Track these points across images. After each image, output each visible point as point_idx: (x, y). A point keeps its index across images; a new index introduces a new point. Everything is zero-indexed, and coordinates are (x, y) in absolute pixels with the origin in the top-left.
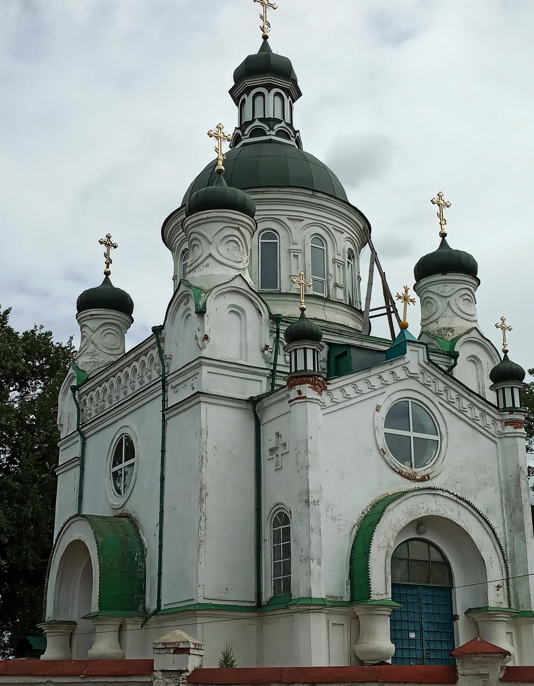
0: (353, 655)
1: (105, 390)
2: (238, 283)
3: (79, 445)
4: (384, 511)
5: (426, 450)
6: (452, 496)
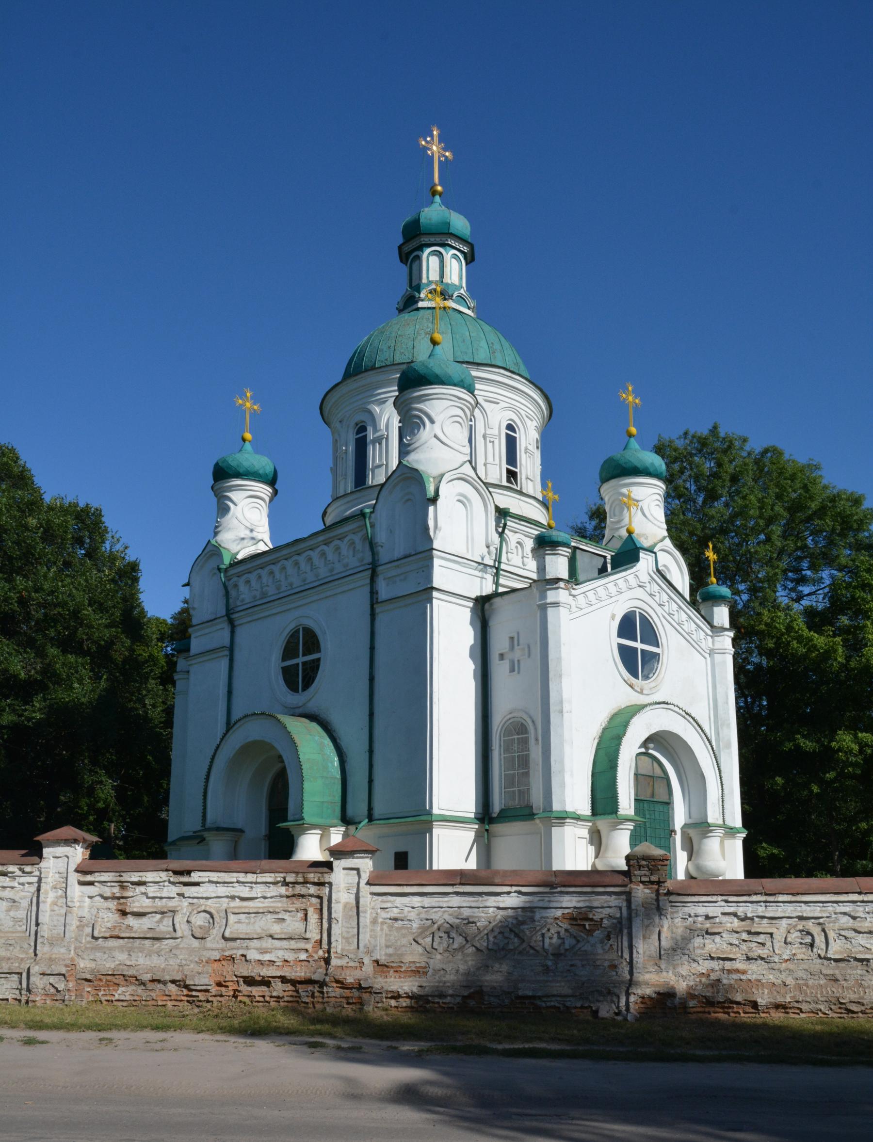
3: (227, 633)
6: (681, 711)
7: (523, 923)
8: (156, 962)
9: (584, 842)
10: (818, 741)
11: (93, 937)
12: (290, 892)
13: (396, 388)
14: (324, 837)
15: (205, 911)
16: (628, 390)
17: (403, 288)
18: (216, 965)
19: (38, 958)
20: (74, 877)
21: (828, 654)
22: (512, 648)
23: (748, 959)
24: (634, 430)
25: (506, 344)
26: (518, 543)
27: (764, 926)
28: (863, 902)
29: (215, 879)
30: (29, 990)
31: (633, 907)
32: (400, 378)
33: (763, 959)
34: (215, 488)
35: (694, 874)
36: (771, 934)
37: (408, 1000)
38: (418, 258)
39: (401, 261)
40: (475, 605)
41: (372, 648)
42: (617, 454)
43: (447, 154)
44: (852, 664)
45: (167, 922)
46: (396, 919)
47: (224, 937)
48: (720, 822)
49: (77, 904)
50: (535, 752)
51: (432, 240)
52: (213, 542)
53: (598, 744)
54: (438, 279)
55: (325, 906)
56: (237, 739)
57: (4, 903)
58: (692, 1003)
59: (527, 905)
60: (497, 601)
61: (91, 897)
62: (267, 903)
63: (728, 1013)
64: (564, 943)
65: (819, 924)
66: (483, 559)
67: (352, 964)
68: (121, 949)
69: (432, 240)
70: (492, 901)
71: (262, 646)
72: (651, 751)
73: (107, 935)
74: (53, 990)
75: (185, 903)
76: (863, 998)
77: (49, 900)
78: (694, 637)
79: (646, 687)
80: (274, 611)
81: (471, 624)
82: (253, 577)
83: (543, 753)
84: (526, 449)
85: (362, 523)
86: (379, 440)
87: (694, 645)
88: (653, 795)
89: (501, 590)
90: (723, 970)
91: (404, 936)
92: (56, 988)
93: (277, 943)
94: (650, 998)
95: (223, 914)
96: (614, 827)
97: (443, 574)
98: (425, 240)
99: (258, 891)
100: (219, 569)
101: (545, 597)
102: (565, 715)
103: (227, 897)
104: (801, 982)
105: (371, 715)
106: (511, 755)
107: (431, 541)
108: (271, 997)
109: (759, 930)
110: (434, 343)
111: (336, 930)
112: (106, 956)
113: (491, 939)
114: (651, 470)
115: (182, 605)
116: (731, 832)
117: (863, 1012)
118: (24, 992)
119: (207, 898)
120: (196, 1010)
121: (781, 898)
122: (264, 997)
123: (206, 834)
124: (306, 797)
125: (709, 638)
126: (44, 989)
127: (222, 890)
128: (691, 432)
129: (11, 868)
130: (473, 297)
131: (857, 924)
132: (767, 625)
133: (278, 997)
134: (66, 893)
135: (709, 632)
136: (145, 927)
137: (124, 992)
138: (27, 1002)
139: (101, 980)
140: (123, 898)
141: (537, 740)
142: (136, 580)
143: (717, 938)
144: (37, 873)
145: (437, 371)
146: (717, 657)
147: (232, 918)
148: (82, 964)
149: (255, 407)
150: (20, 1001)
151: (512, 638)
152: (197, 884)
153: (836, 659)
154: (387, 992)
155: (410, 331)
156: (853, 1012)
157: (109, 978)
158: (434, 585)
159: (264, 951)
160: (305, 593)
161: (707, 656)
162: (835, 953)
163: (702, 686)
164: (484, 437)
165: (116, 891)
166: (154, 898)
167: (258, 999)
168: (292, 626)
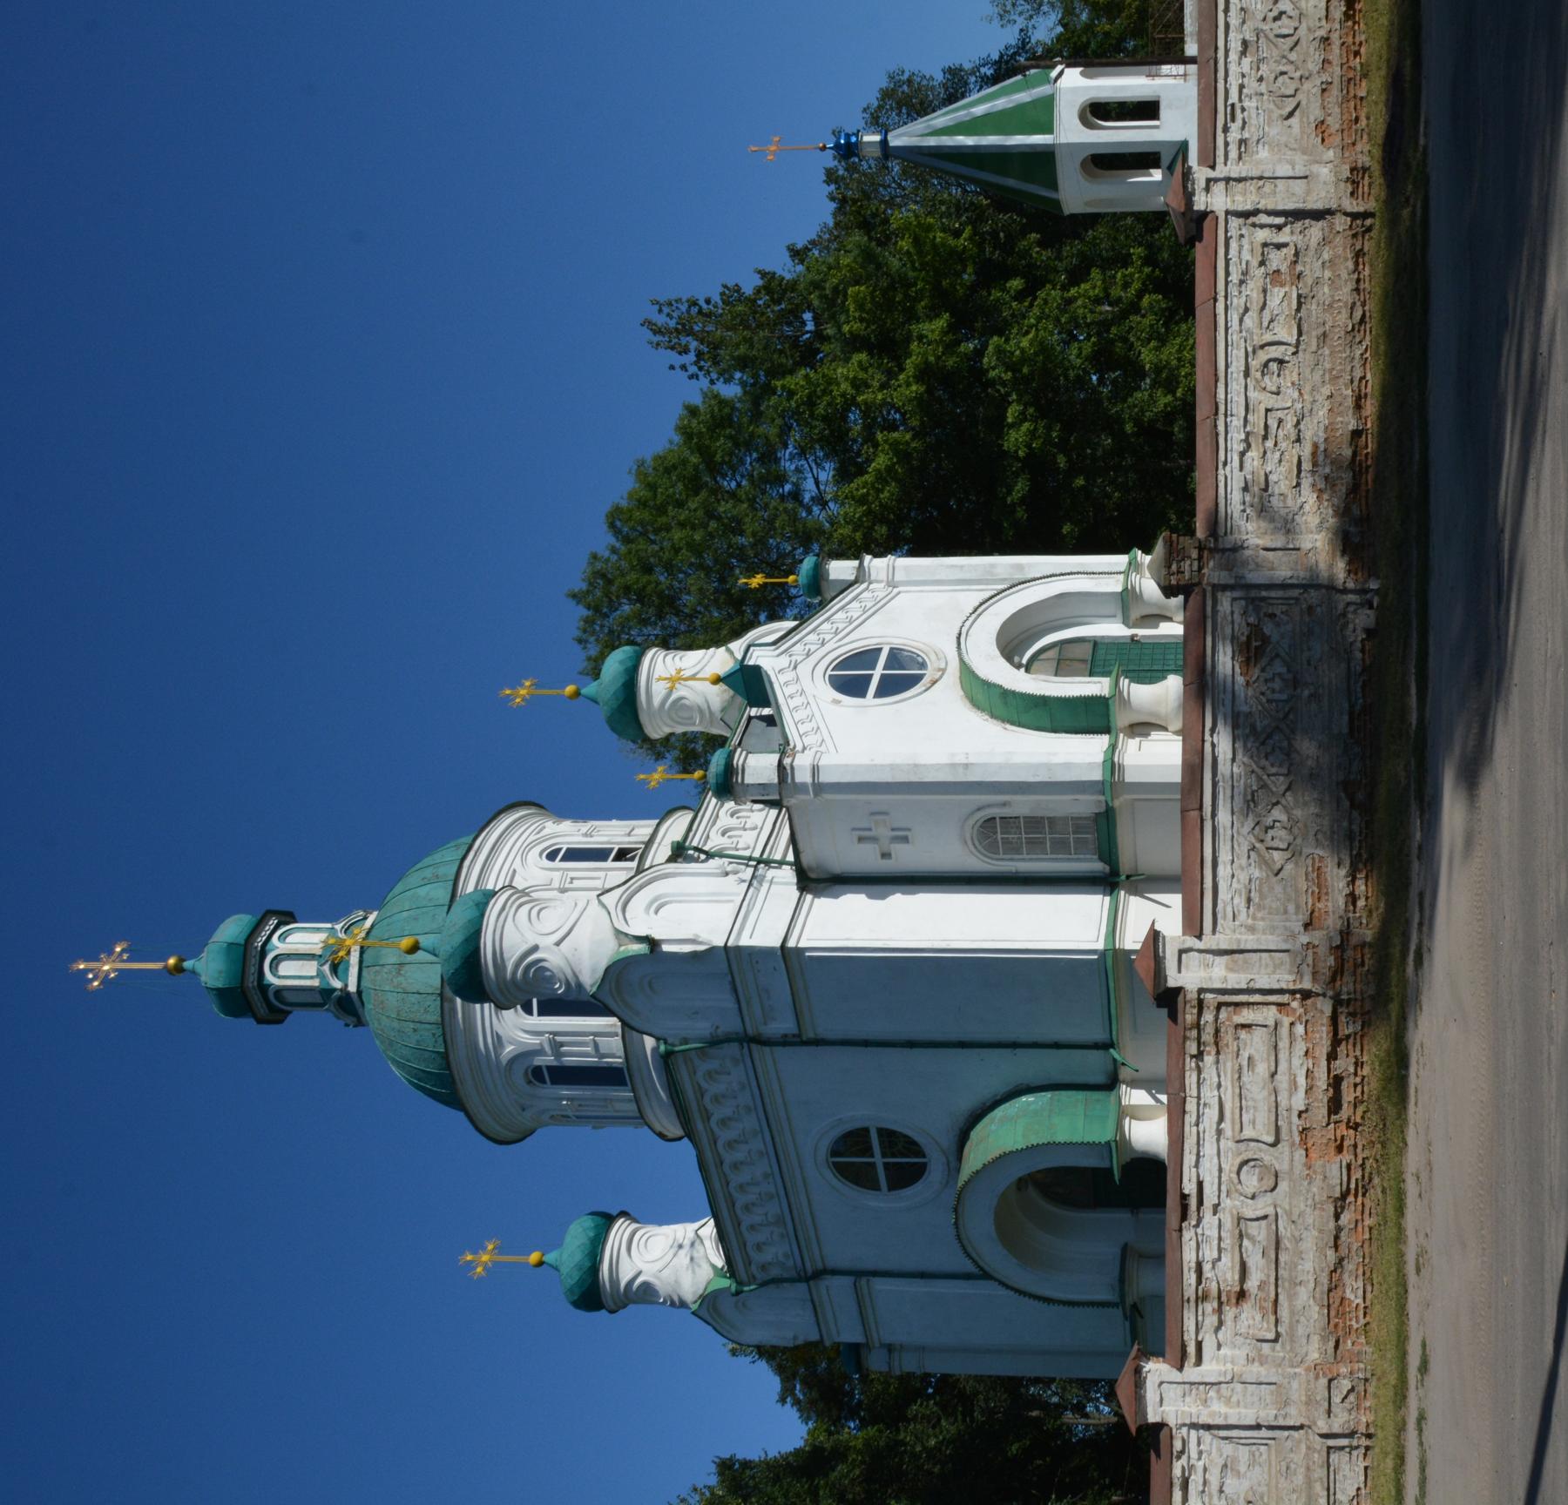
7: (1253, 727)
8: (1309, 1243)
9: (1146, 744)
10: (1016, 475)
11: (1275, 1340)
12: (1211, 1049)
13: (478, 1006)
14: (1137, 1113)
15: (1238, 1173)
17: (325, 1019)
18: (1313, 1155)
19: (1306, 1423)
20: (1191, 1373)
21: (902, 454)
22: (874, 839)
23: (1298, 440)
24: (570, 689)
25: (427, 861)
26: (723, 834)
27: (1257, 419)
28: (1226, 297)
29: (1194, 1158)
30: (1351, 1435)
31: (1232, 581)
32: (464, 998)
33: (1298, 423)
34: (613, 1307)
36: (1267, 410)
37: (1358, 883)
38: (279, 991)
39: (280, 1022)
40: (809, 891)
41: (866, 1043)
42: (603, 712)
44: (915, 423)
45: (1253, 1228)
46: (1249, 900)
47: (1274, 1145)
48: (1121, 577)
49: (1229, 1366)
50: (1022, 806)
51: (253, 970)
52: (694, 1307)
53: (1012, 723)
54: (315, 963)
55: (1231, 999)
56: (994, 1256)
57: (1228, 1481)
58: (1356, 511)
59: (1229, 721)
60: (806, 860)
61: (1219, 1346)
62: (1227, 1083)
63: (1368, 467)
64: (1280, 674)
65: (1254, 352)
67: (1310, 960)
68: (1292, 1297)
69: (253, 970)
70: (1224, 768)
71: (855, 1224)
72: (1024, 661)
73: (1272, 1318)
74: (1352, 1398)
75: (1227, 1203)
77: (1224, 1409)
79: (936, 665)
80: (805, 1204)
81: (836, 897)
82: (752, 1239)
83: (1023, 793)
84: (586, 835)
85: (680, 1059)
86: (556, 1046)
87: (879, 606)
88: (1084, 661)
89: (790, 857)
90: (1313, 472)
91: (1271, 889)
92: (1349, 1392)
93: (1283, 1067)
94: (1349, 563)
95: (1242, 1146)
96: (1126, 703)
97: (764, 933)
98: (251, 980)
99: (1209, 1095)
100: (738, 1293)
101: (804, 785)
102: (972, 760)
103: (1218, 1140)
105: (962, 1045)
106: (1025, 841)
107: (713, 949)
108: (1356, 1074)
110: (415, 948)
111: (1263, 982)
112: (1302, 1319)
113: (1274, 770)
114: (630, 664)
115: (788, 1405)
117: (1363, 305)
118: (1355, 1443)
119: (1220, 1170)
120: (1376, 1180)
122: (1356, 1085)
123: (1129, 1301)
124: (1077, 1139)
126: (1350, 1411)
127: (1209, 1149)
128: (578, 633)
129: (1177, 1472)
130: (348, 913)
131: (1255, 307)
132: (855, 530)
133: (1356, 1064)
134: (1213, 1384)
135: (864, 586)
136: (1262, 1262)
137: (1353, 1291)
138: (1369, 1436)
139: (1336, 1326)
140: (1219, 1297)
141: (1004, 804)
142: (746, 1464)
143: (1273, 478)
144: (1185, 1430)
145: (458, 939)
147: (1248, 1133)
148: (1314, 1356)
149: (490, 1247)
150: (1367, 1448)
152: (1200, 1184)
153: (907, 443)
154: (1346, 911)
155: (392, 1000)
156: (1364, 316)
157: (1333, 1313)
158: (778, 944)
159: (1294, 1084)
160: (780, 1153)
163: (937, 598)
165: (1210, 1307)
166: (1220, 1250)
167: (1358, 1093)
168: (830, 1175)
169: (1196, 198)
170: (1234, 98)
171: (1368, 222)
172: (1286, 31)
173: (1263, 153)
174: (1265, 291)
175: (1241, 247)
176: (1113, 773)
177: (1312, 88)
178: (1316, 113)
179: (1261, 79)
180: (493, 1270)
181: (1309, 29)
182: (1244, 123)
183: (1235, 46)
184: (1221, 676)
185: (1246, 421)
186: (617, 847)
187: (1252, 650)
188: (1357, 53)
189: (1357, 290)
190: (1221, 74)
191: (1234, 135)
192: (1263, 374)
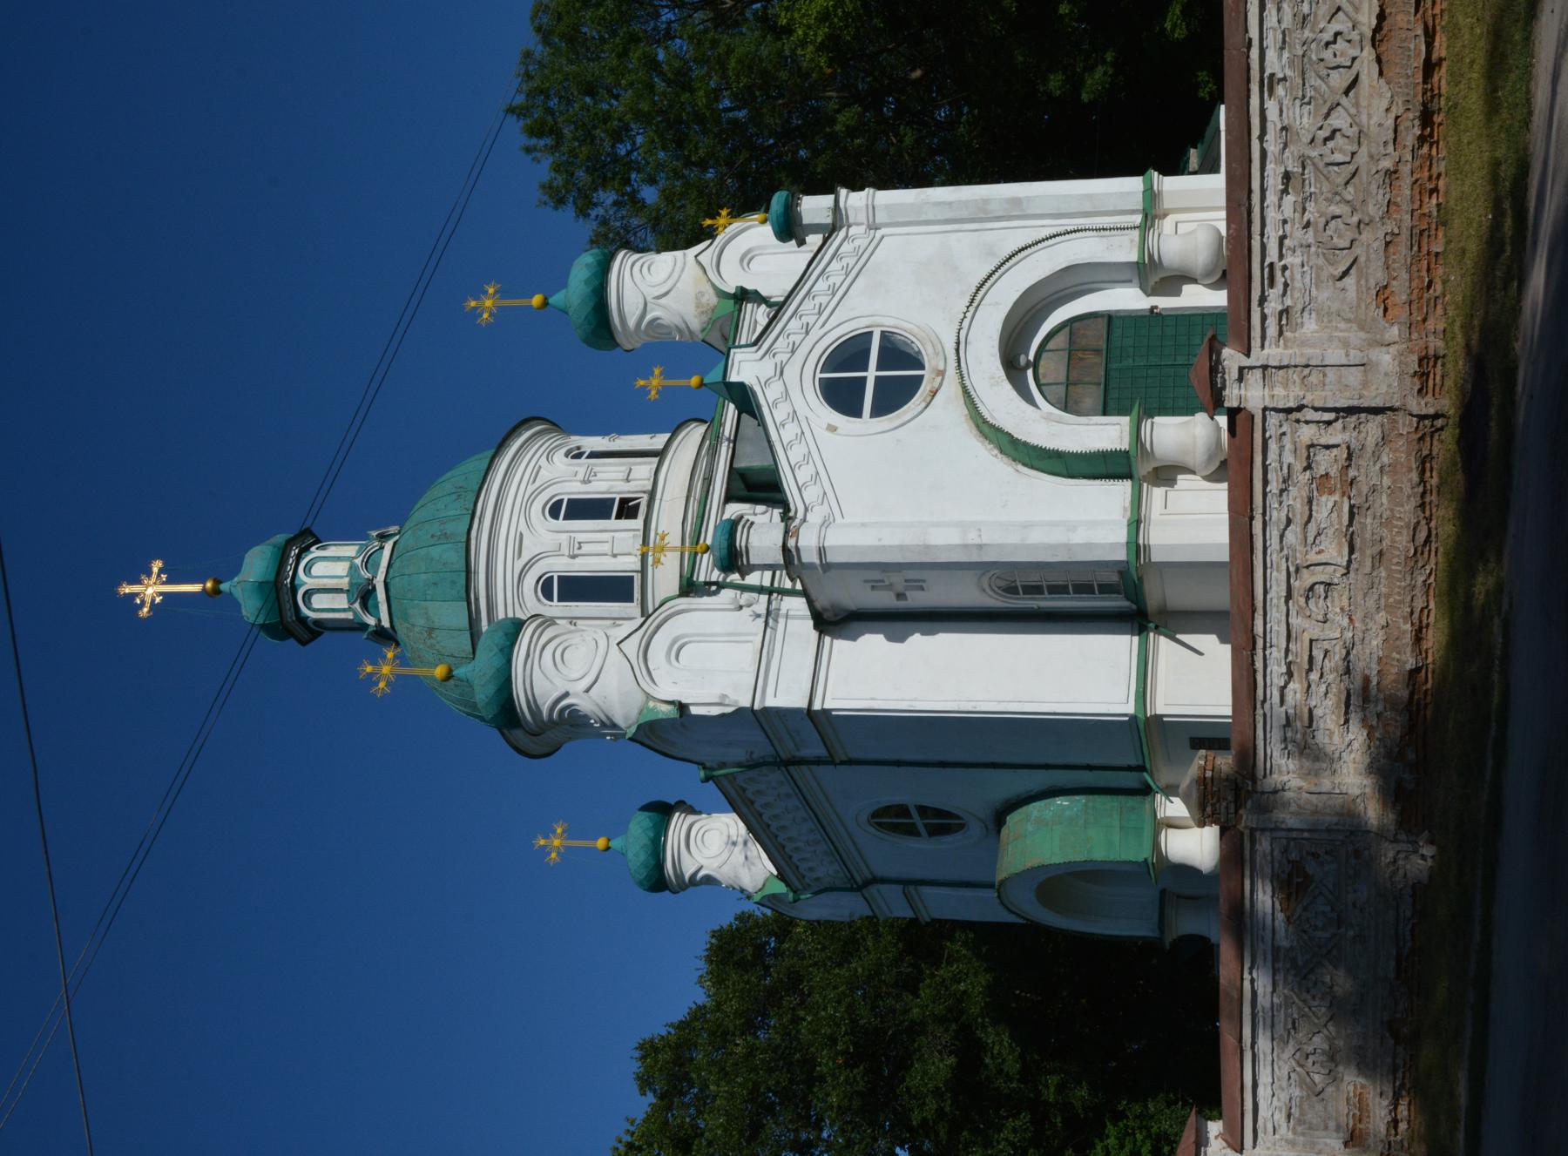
0: (1213, 478)
1: (797, 849)
2: (631, 647)
3: (884, 888)
4: (992, 426)
5: (898, 353)
6: (969, 315)
16: (475, 308)
27: (1300, 649)
33: (1348, 653)
35: (1219, 275)
37: (1400, 1108)
41: (898, 763)
43: (155, 570)
46: (1289, 1116)
48: (1136, 233)
53: (1024, 465)
65: (1297, 570)
66: (758, 616)
72: (1031, 357)
76: (1408, 526)
78: (852, 262)
81: (854, 639)
88: (1097, 351)
98: (290, 616)
102: (985, 540)
104: (1383, 601)
107: (740, 711)
109: (1306, 658)
116: (1151, 212)
117: (1429, 520)
121: (1259, 629)
125: (852, 231)
131: (1299, 520)
135: (842, 234)
143: (1318, 712)
146: (881, 218)
149: (491, 291)
151: (873, 588)
154: (1388, 1134)
161: (879, 234)
162: (1340, 552)
163: (925, 244)
164: (574, 557)
169: (1227, 392)
170: (1272, 255)
171: (1439, 423)
172: (1339, 157)
173: (1310, 325)
174: (1310, 502)
175: (1282, 448)
176: (1138, 557)
177: (1372, 239)
178: (1377, 275)
179: (1308, 225)
180: (500, 313)
181: (1371, 157)
182: (1286, 285)
183: (1274, 182)
184: (1260, 914)
185: (1287, 650)
186: (618, 497)
187: (1291, 884)
188: (1435, 190)
189: (1422, 506)
190: (1256, 227)
191: (1273, 306)
192: (1307, 598)
